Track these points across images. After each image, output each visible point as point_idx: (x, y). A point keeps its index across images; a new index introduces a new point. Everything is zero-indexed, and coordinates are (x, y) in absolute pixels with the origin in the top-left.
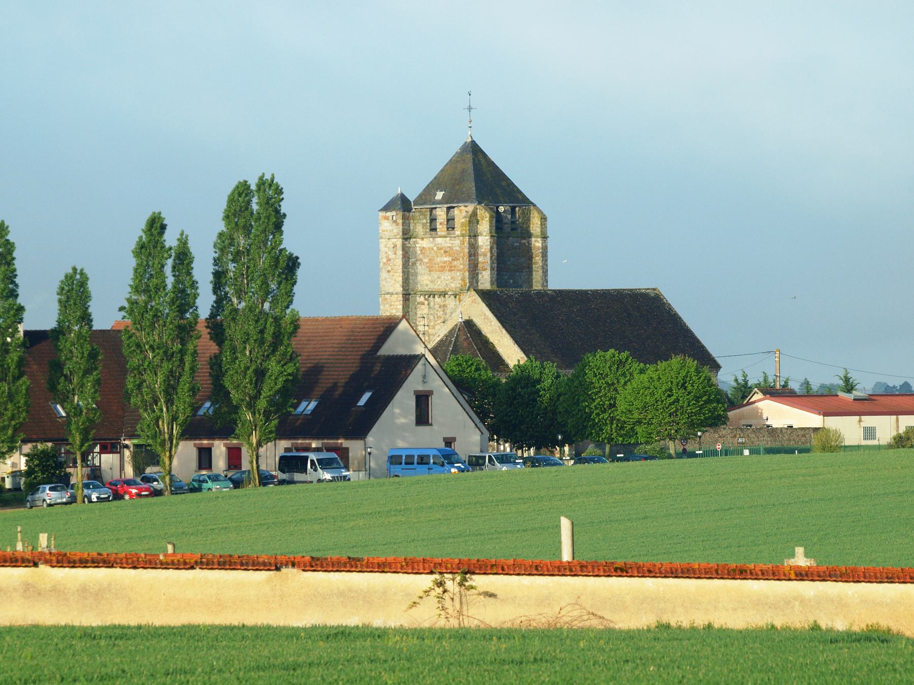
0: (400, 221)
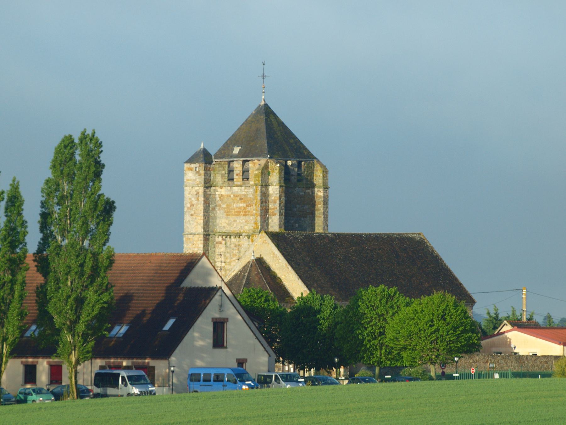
0: (202, 172)
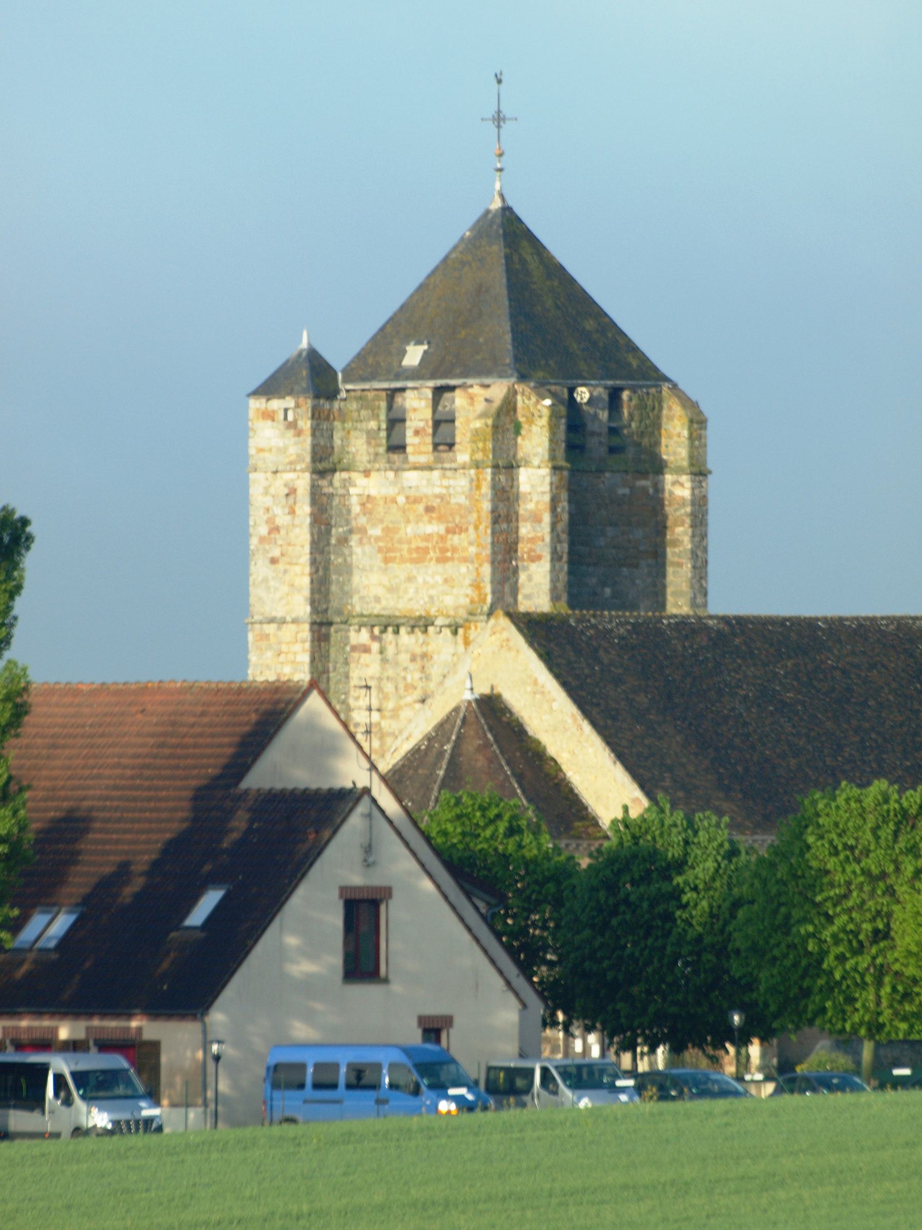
0: (306, 424)
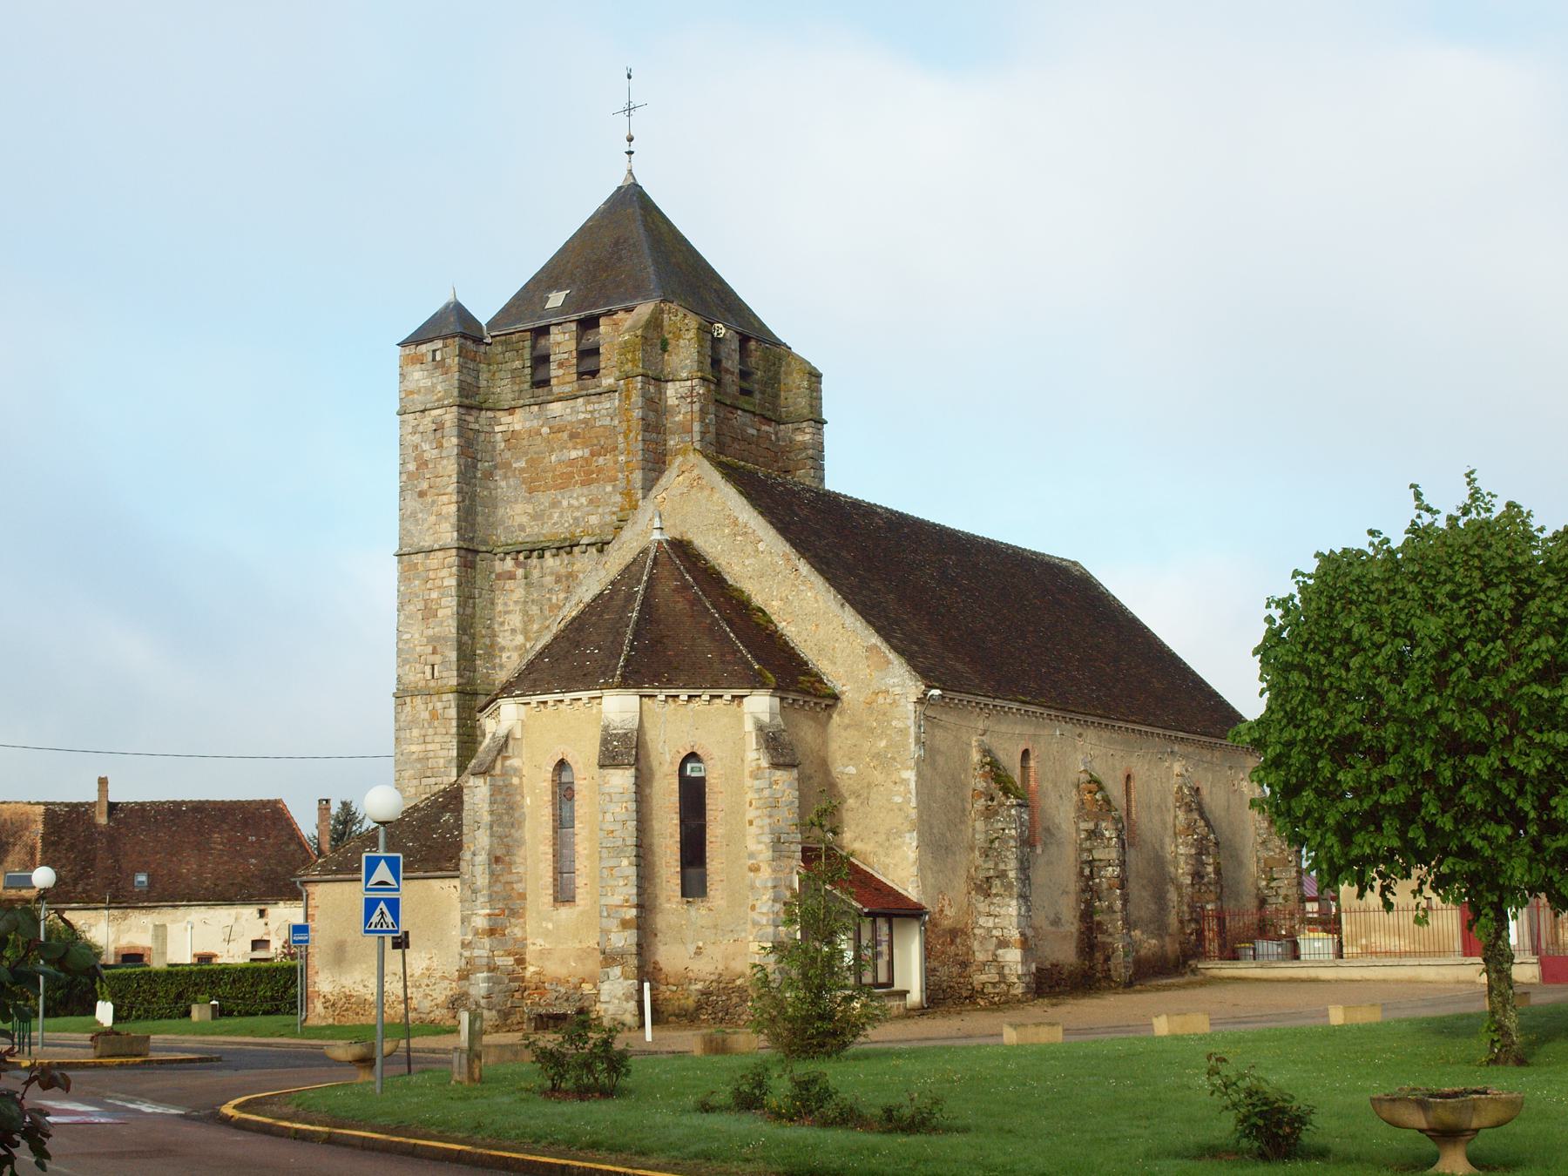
0: (454, 362)
